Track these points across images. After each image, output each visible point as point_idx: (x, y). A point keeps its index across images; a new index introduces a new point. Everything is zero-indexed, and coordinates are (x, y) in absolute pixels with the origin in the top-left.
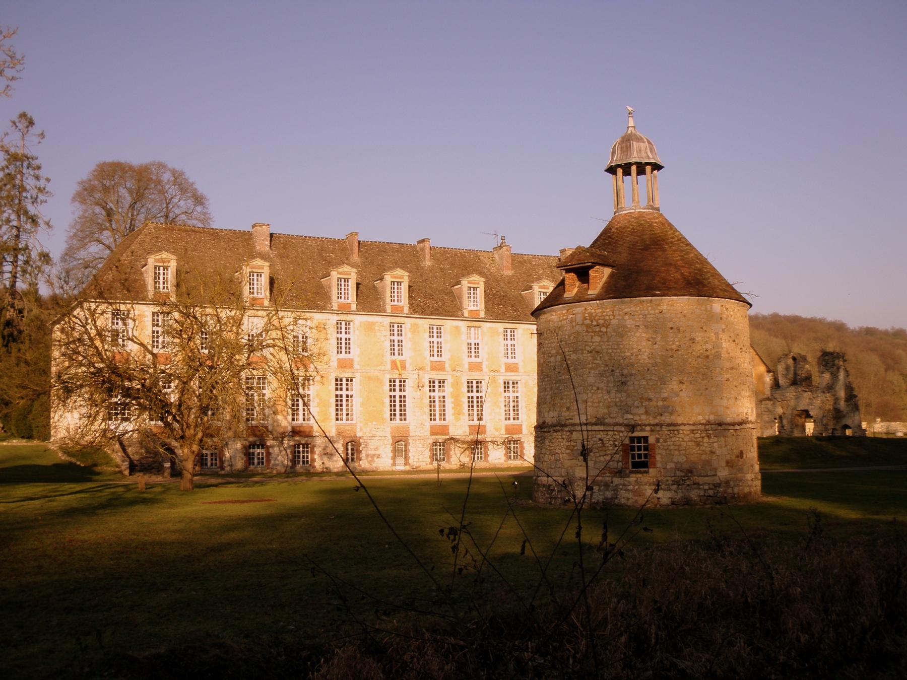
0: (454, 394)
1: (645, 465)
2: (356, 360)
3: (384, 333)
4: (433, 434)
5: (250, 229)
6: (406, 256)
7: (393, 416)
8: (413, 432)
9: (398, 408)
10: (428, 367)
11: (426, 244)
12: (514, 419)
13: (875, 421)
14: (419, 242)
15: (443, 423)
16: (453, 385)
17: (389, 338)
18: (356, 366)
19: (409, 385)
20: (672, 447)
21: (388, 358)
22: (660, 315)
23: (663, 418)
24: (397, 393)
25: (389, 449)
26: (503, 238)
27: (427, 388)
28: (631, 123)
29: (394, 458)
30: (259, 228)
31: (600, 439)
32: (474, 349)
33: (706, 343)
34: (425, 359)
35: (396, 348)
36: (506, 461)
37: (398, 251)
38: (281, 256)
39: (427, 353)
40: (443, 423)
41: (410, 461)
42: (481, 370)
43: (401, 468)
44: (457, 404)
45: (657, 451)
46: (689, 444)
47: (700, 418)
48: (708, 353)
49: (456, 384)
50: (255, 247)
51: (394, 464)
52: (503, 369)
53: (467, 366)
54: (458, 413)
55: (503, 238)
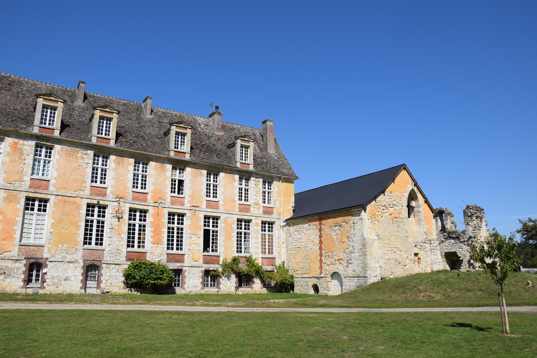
2: (221, 203)
3: (87, 161)
4: (206, 262)
7: (87, 241)
8: (107, 258)
9: (94, 233)
10: (130, 197)
12: (213, 251)
13: (253, 283)
16: (153, 216)
18: (51, 188)
24: (176, 225)
27: (126, 216)
32: (179, 186)
34: (128, 189)
35: (243, 195)
36: (202, 289)
39: (237, 198)
41: (102, 285)
42: (183, 205)
44: (157, 232)
49: (158, 215)
52: (204, 206)
53: (169, 199)
54: (156, 242)
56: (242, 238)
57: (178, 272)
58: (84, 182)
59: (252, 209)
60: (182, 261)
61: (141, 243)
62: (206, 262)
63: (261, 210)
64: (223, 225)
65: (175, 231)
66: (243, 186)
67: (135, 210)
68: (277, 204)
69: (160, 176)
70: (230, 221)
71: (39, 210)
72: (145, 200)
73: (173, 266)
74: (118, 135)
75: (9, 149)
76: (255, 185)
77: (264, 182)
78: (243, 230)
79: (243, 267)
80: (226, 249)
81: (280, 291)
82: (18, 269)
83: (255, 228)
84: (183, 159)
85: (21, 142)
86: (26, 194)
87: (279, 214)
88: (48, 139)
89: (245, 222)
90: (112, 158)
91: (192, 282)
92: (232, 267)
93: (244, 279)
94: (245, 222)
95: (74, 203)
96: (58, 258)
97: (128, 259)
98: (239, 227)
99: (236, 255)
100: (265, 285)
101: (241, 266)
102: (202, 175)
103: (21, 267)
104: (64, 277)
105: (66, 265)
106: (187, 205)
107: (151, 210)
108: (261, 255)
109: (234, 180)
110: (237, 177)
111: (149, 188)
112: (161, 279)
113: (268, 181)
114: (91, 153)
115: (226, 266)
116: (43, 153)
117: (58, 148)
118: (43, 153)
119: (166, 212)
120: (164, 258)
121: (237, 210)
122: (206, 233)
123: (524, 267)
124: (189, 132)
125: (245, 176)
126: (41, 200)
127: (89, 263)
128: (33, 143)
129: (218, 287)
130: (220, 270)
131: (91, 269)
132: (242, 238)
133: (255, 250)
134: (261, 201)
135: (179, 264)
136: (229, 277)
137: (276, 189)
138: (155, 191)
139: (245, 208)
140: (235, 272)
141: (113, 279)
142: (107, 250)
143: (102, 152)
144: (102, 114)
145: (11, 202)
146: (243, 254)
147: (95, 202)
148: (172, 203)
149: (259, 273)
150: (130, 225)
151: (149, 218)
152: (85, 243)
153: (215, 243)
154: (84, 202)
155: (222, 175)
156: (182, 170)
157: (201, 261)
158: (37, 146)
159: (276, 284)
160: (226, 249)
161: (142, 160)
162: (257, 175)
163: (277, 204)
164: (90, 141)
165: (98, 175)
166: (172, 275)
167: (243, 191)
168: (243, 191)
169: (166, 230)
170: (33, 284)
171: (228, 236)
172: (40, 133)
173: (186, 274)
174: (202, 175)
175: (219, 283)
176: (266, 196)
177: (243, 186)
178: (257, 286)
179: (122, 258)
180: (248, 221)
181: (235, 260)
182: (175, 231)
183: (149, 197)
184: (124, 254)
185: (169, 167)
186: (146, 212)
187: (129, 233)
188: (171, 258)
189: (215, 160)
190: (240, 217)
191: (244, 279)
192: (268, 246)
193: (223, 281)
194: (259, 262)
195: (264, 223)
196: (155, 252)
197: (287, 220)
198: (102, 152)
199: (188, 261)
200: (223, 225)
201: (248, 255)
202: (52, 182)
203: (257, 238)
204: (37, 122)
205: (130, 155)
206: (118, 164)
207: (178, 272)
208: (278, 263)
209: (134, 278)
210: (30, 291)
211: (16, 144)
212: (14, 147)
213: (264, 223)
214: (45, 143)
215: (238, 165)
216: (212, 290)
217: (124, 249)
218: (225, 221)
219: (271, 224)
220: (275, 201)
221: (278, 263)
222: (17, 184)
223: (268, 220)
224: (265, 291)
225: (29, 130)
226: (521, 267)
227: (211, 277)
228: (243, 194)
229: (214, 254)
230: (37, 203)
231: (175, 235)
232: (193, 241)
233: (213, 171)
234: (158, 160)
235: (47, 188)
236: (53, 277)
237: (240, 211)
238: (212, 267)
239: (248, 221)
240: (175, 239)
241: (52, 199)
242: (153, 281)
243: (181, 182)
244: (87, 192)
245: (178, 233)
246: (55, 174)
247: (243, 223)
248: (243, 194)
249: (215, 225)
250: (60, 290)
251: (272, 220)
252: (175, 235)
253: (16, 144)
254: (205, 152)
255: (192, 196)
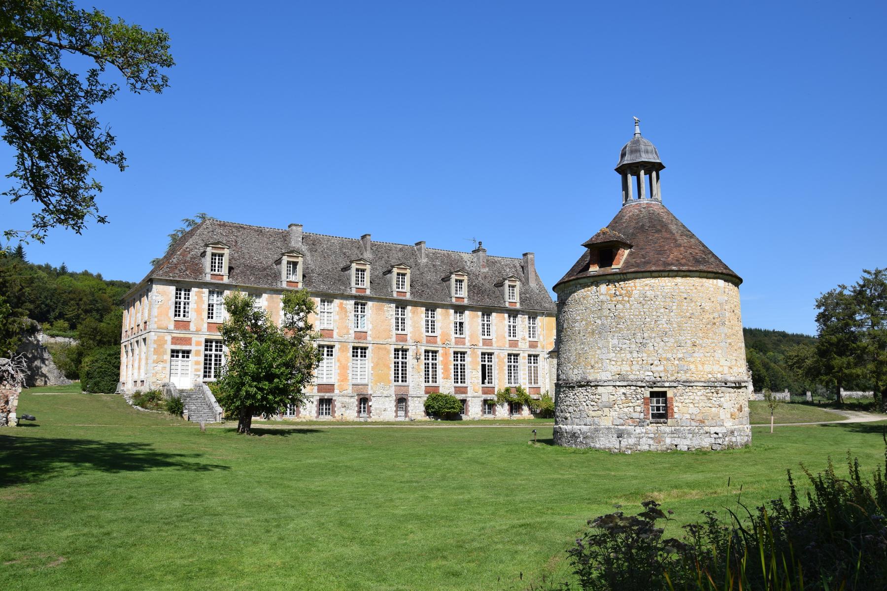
0: (444, 363)
1: (664, 416)
3: (391, 313)
4: (484, 393)
5: (287, 229)
6: (410, 256)
8: (411, 392)
9: (401, 373)
10: (424, 341)
11: (423, 245)
14: (417, 244)
15: (434, 384)
16: (443, 355)
17: (395, 316)
18: (369, 338)
19: (410, 354)
20: (687, 401)
21: (394, 332)
22: (676, 287)
23: (679, 375)
25: (393, 404)
26: (480, 243)
27: (423, 357)
28: (638, 130)
29: (396, 411)
30: (294, 228)
31: (624, 394)
33: (714, 312)
36: (317, 417)
37: (401, 250)
38: (311, 250)
39: (424, 330)
40: (434, 384)
41: (409, 414)
42: (464, 344)
43: (402, 419)
44: (446, 370)
45: (675, 404)
46: (702, 398)
47: (719, 376)
48: (715, 321)
49: (446, 355)
50: (290, 242)
51: (397, 416)
52: (481, 344)
53: (453, 340)
54: (446, 378)
55: (480, 243)
56: (512, 370)
57: (464, 401)
58: (390, 331)
59: (519, 344)
60: (466, 393)
61: (516, 379)
62: (484, 393)
63: (528, 344)
64: (497, 360)
65: (213, 358)
66: (512, 324)
67: (357, 348)
68: (541, 337)
69: (445, 319)
70: (502, 355)
71: (328, 355)
72: (436, 343)
73: (460, 397)
74: (231, 269)
75: (337, 309)
76: (522, 321)
77: (529, 318)
78: (214, 352)
79: (514, 396)
80: (500, 382)
81: (545, 417)
82: (353, 403)
83: (523, 361)
84: (221, 282)
85: (345, 302)
86: (353, 345)
87: (543, 348)
88: (362, 298)
89: (328, 347)
90: (409, 308)
91: (474, 411)
92: (505, 396)
93: (515, 407)
94: (328, 347)
95: (386, 349)
96: (378, 393)
97: (426, 393)
98: (483, 360)
99: (508, 385)
100: (533, 412)
101: (512, 395)
102: (478, 316)
103: (354, 401)
104: (384, 410)
105: (383, 399)
106: (468, 344)
107: (441, 351)
108: (528, 385)
109: (504, 319)
110: (506, 315)
111: (438, 332)
112: (453, 408)
113: (533, 316)
114: (393, 306)
115: (500, 396)
116: (183, 296)
117: (370, 304)
118: (183, 296)
119: (452, 351)
120: (452, 390)
121: (507, 346)
122: (483, 366)
123: (845, 390)
124: (466, 278)
125: (513, 314)
126: (362, 348)
127: (399, 397)
128: (353, 302)
129: (494, 413)
130: (496, 399)
131: (401, 401)
132: (512, 370)
133: (523, 381)
134: (527, 336)
135: (463, 395)
136: (502, 405)
137: (540, 324)
138: (443, 334)
139: (514, 344)
140: (507, 401)
141: (417, 409)
142: (411, 385)
143: (402, 305)
144: (358, 267)
145: (343, 351)
146: (513, 385)
147: (400, 347)
148: (456, 343)
149: (527, 402)
150: (206, 356)
151: (439, 357)
152: (205, 376)
153: (490, 376)
154: (392, 348)
155: (494, 314)
156: (462, 313)
157: (480, 392)
158: (356, 304)
159: (541, 411)
160: (500, 382)
161: (431, 308)
162: (523, 312)
163: (541, 337)
164: (392, 296)
165: (400, 323)
166: (461, 404)
167: (400, 321)
168: (400, 321)
169: (453, 367)
170: (362, 415)
171: (501, 369)
172: (358, 294)
173: (469, 403)
174: (478, 316)
175: (494, 411)
176: (532, 331)
177: (512, 324)
178: (526, 412)
179: (422, 392)
180: (517, 355)
181: (507, 390)
182: (213, 358)
183: (438, 339)
184: (423, 388)
185: (452, 311)
186: (436, 352)
187: (205, 364)
188: (458, 390)
189: (488, 302)
190: (510, 352)
191: (515, 407)
192: (534, 376)
193: (498, 408)
194: (527, 391)
195: (530, 356)
196: (446, 386)
197: (550, 353)
198: (402, 305)
199: (470, 393)
200: (497, 360)
201: (517, 385)
202: (369, 333)
203: (524, 370)
204: (353, 284)
205: (422, 305)
206: (414, 313)
207: (464, 401)
208: (543, 391)
209: (433, 408)
210: (362, 420)
211: (341, 304)
212: (341, 306)
213: (530, 356)
214: (360, 301)
215: (507, 305)
216: (490, 417)
217: (423, 384)
218: (498, 356)
219: (536, 356)
220: (539, 335)
221: (543, 391)
222: (346, 336)
223: (534, 353)
224: (532, 417)
225: (279, 286)
226: (842, 390)
227: (489, 405)
228: (513, 331)
229: (490, 385)
230: (214, 344)
231: (213, 362)
232: (473, 375)
233: (487, 312)
234: (443, 306)
235: (366, 338)
236: (376, 409)
237: (510, 346)
238: (489, 397)
239: (517, 355)
240: (460, 374)
241: (370, 346)
242: (444, 409)
243: (461, 324)
244: (394, 339)
245: (216, 360)
246: (370, 326)
247: (359, 351)
248: (513, 331)
249: (490, 361)
250: (381, 419)
251: (537, 353)
252: (213, 362)
253: (341, 304)
254: (478, 294)
255: (471, 336)
